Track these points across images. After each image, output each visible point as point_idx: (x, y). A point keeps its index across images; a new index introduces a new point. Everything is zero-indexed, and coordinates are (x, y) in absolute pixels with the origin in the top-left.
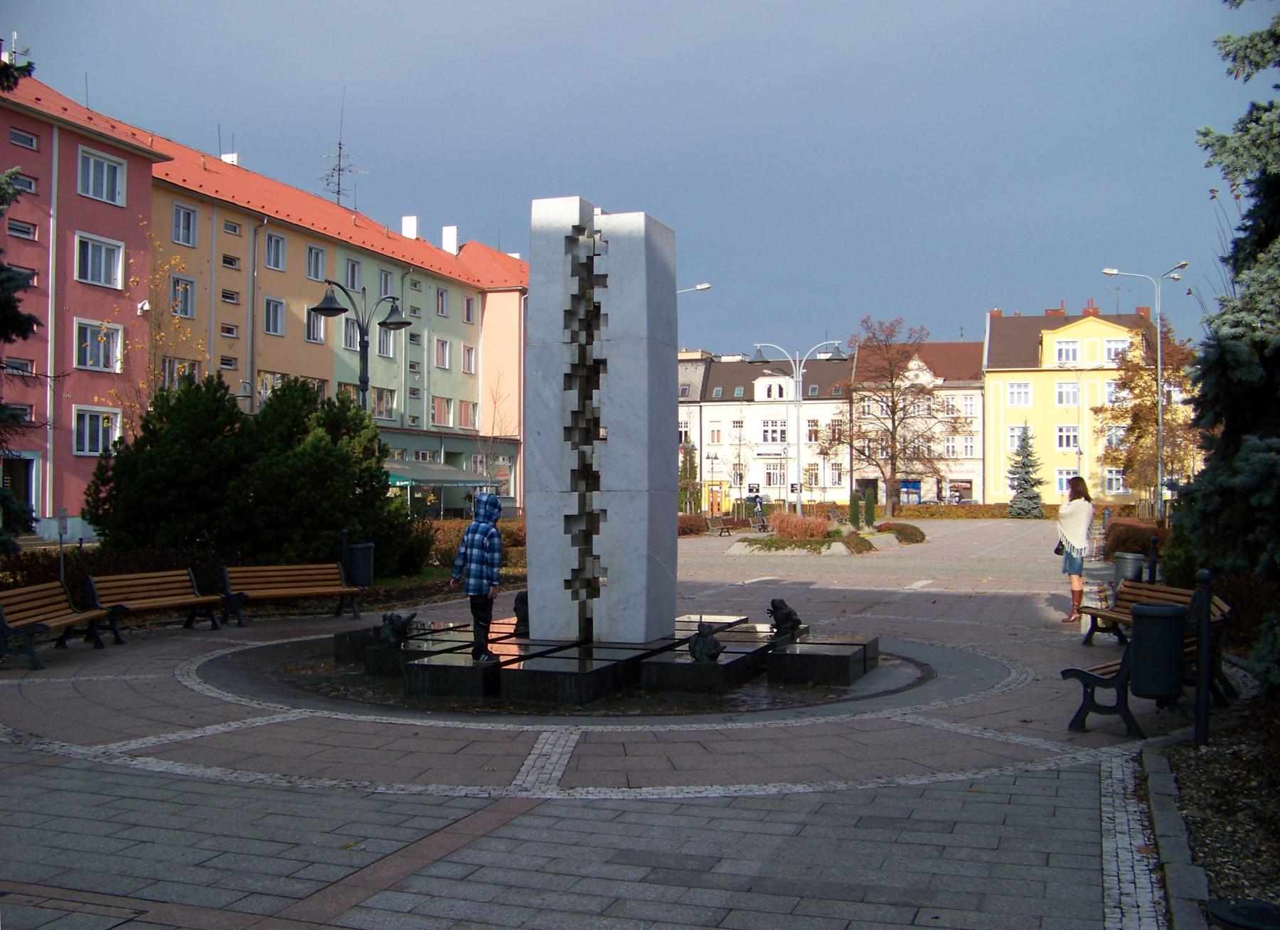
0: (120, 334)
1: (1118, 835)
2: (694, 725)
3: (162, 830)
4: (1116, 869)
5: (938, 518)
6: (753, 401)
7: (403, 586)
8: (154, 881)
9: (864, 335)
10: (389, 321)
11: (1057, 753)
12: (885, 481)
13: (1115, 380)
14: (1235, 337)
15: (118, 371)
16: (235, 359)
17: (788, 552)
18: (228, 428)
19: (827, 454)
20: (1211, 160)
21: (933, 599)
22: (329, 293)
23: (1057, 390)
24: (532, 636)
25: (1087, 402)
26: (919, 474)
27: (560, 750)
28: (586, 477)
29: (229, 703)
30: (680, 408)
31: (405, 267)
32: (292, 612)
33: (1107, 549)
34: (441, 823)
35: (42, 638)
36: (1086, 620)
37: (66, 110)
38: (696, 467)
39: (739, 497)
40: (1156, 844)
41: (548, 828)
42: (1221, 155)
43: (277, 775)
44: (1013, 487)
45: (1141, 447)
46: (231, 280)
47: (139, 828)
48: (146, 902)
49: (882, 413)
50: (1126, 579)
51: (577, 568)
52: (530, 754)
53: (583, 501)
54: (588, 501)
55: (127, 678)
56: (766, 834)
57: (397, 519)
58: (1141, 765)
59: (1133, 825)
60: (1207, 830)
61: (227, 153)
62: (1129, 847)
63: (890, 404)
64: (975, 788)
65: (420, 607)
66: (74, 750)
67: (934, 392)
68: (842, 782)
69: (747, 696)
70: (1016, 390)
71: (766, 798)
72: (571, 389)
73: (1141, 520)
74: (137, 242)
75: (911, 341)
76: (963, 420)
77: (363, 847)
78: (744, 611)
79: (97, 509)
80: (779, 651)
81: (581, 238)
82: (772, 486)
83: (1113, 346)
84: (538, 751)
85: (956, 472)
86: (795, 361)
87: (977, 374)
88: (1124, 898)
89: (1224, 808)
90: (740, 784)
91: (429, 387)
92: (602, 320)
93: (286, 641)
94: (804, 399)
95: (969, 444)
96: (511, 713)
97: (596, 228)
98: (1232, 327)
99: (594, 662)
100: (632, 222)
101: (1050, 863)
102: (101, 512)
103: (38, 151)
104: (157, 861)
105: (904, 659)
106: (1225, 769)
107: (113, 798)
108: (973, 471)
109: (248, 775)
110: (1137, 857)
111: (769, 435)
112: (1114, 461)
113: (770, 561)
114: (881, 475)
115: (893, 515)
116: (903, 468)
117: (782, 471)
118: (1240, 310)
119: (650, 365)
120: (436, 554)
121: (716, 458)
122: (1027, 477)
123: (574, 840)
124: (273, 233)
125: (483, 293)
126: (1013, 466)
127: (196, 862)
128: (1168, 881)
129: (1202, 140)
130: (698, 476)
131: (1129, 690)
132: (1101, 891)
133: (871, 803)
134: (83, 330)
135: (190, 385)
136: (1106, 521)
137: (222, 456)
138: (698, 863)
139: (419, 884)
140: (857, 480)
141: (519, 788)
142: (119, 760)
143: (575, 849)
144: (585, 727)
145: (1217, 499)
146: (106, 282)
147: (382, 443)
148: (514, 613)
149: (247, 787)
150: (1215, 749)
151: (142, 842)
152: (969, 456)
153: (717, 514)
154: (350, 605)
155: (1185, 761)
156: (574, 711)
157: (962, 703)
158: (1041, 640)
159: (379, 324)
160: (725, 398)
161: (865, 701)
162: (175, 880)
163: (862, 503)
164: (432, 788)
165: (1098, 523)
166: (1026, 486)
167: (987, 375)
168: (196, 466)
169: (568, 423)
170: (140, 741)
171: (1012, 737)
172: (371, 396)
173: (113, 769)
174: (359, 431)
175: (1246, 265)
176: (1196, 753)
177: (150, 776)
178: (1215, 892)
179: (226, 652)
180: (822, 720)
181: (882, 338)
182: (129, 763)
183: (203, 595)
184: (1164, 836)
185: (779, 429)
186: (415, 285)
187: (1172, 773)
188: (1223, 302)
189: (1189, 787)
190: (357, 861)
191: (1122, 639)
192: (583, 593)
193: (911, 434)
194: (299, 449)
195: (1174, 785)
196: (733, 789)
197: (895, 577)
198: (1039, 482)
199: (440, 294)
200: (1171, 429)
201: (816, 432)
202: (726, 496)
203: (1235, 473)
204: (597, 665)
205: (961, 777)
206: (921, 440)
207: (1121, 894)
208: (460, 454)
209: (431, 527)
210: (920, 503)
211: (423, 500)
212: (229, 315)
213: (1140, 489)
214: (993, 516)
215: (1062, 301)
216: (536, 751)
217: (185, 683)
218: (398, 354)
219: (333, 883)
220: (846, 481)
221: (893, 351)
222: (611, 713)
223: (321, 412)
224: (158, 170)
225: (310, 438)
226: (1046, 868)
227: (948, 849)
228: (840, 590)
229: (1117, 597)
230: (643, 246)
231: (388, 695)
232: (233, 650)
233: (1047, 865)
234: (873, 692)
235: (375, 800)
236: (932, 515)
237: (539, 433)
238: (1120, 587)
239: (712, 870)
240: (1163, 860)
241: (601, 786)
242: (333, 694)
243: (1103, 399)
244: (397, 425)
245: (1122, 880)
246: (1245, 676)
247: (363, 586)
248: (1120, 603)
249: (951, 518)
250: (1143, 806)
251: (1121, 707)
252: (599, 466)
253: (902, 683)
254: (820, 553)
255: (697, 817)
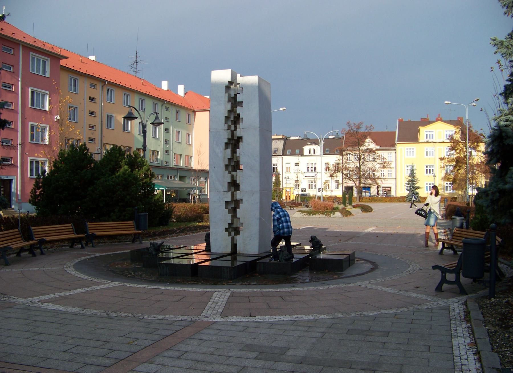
0: (48, 128)
1: (459, 338)
2: (278, 289)
3: (52, 336)
4: (459, 353)
5: (378, 202)
6: (303, 155)
7: (161, 230)
8: (46, 359)
9: (347, 129)
10: (154, 122)
11: (431, 301)
12: (356, 187)
13: (449, 147)
14: (506, 126)
15: (47, 143)
16: (94, 138)
17: (317, 216)
18: (88, 166)
19: (333, 176)
20: (497, 51)
21: (377, 236)
22: (130, 111)
23: (425, 151)
24: (212, 251)
25: (438, 155)
26: (370, 184)
27: (222, 300)
28: (234, 185)
29: (85, 279)
30: (273, 158)
31: (163, 101)
32: (114, 241)
33: (447, 215)
34: (170, 332)
35: (11, 252)
36: (441, 244)
37: (25, 38)
38: (280, 182)
39: (297, 194)
40: (476, 342)
41: (216, 335)
42: (501, 49)
43: (102, 311)
44: (407, 190)
45: (460, 173)
46: (93, 107)
47: (42, 335)
48: (41, 368)
49: (355, 160)
50: (457, 227)
51: (230, 223)
52: (209, 302)
53: (233, 195)
54: (235, 195)
55: (44, 269)
56: (308, 337)
57: (158, 203)
58: (466, 306)
59: (465, 333)
60: (497, 336)
61: (91, 55)
62: (464, 343)
63: (358, 156)
64: (397, 316)
65: (167, 239)
66: (19, 300)
67: (376, 152)
68: (341, 314)
69: (301, 276)
70: (409, 151)
71: (308, 321)
72: (228, 149)
73: (460, 203)
74: (54, 92)
75: (367, 131)
76: (388, 163)
77: (136, 343)
78: (299, 240)
79: (35, 199)
80: (314, 257)
81: (232, 86)
82: (311, 189)
83: (448, 133)
84: (213, 300)
85: (385, 183)
86: (320, 139)
87: (393, 144)
88: (463, 367)
89: (503, 326)
90: (298, 315)
91: (173, 150)
92: (240, 120)
93: (111, 253)
94: (324, 155)
95: (390, 173)
96: (202, 284)
97: (238, 82)
98: (505, 122)
99: (237, 262)
100: (253, 79)
101: (430, 350)
102: (37, 200)
103: (14, 55)
104: (48, 350)
105: (366, 260)
106: (503, 309)
107: (32, 321)
108: (392, 183)
109: (90, 311)
110: (468, 348)
111: (310, 169)
112: (449, 179)
113: (310, 219)
114: (355, 185)
115: (359, 201)
116: (363, 182)
117: (315, 183)
118: (508, 115)
119: (260, 139)
120: (174, 217)
121: (288, 178)
122: (413, 185)
123: (226, 340)
124: (109, 88)
125: (195, 112)
126: (408, 181)
127: (64, 350)
128: (482, 359)
129: (493, 42)
130: (281, 185)
131: (461, 273)
132: (453, 364)
133: (353, 323)
134: (32, 127)
135: (73, 149)
136: (446, 203)
137: (86, 177)
138: (279, 350)
139: (159, 360)
140: (345, 187)
141: (204, 317)
142: (38, 304)
143: (227, 344)
144: (233, 290)
145: (498, 194)
146: (42, 108)
147: (152, 172)
148: (205, 242)
149: (90, 316)
150: (498, 300)
151: (43, 341)
152: (390, 177)
153: (289, 201)
154: (138, 238)
155: (485, 305)
156: (229, 283)
157: (390, 279)
158: (421, 252)
159: (123, 118)
160: (292, 154)
161: (349, 278)
162: (55, 358)
163: (347, 196)
164: (167, 317)
165: (442, 204)
166: (413, 189)
167: (397, 145)
168: (75, 181)
169: (227, 163)
170: (47, 296)
171: (412, 294)
172: (148, 154)
173: (34, 309)
174: (142, 167)
175: (510, 96)
176: (490, 301)
177: (49, 312)
178: (503, 364)
179: (86, 258)
180: (332, 287)
181: (355, 130)
182: (41, 306)
183: (78, 234)
184: (479, 338)
185: (313, 166)
186: (167, 109)
187: (480, 310)
188: (501, 111)
189: (488, 316)
190: (133, 350)
191: (455, 252)
192: (233, 233)
193: (367, 168)
194: (117, 174)
195: (481, 316)
196: (294, 317)
197: (361, 226)
198: (418, 188)
199: (177, 112)
200: (472, 167)
201: (329, 168)
202: (292, 193)
203: (506, 183)
204: (238, 263)
205: (391, 312)
206: (371, 171)
207: (462, 365)
208: (185, 177)
209: (172, 206)
210: (370, 196)
211: (171, 195)
212: (91, 121)
213: (459, 190)
214: (400, 201)
215: (428, 115)
216: (212, 300)
217: (68, 271)
218: (160, 136)
219: (122, 360)
220: (340, 187)
221: (359, 135)
222: (243, 284)
223: (127, 159)
224: (63, 62)
225: (122, 170)
226: (429, 353)
227: (386, 344)
228: (339, 231)
229: (453, 235)
230: (257, 90)
231: (152, 276)
232: (89, 257)
233: (429, 351)
234: (353, 275)
235: (142, 322)
236: (375, 201)
237: (214, 167)
238: (454, 230)
239: (286, 354)
240: (479, 349)
241: (239, 316)
242: (129, 275)
243: (444, 154)
244: (160, 165)
245: (462, 358)
246: (507, 268)
247: (143, 230)
248: (454, 237)
249: (383, 202)
250: (469, 325)
251: (457, 281)
252: (239, 181)
253: (365, 270)
254: (330, 216)
255: (279, 329)
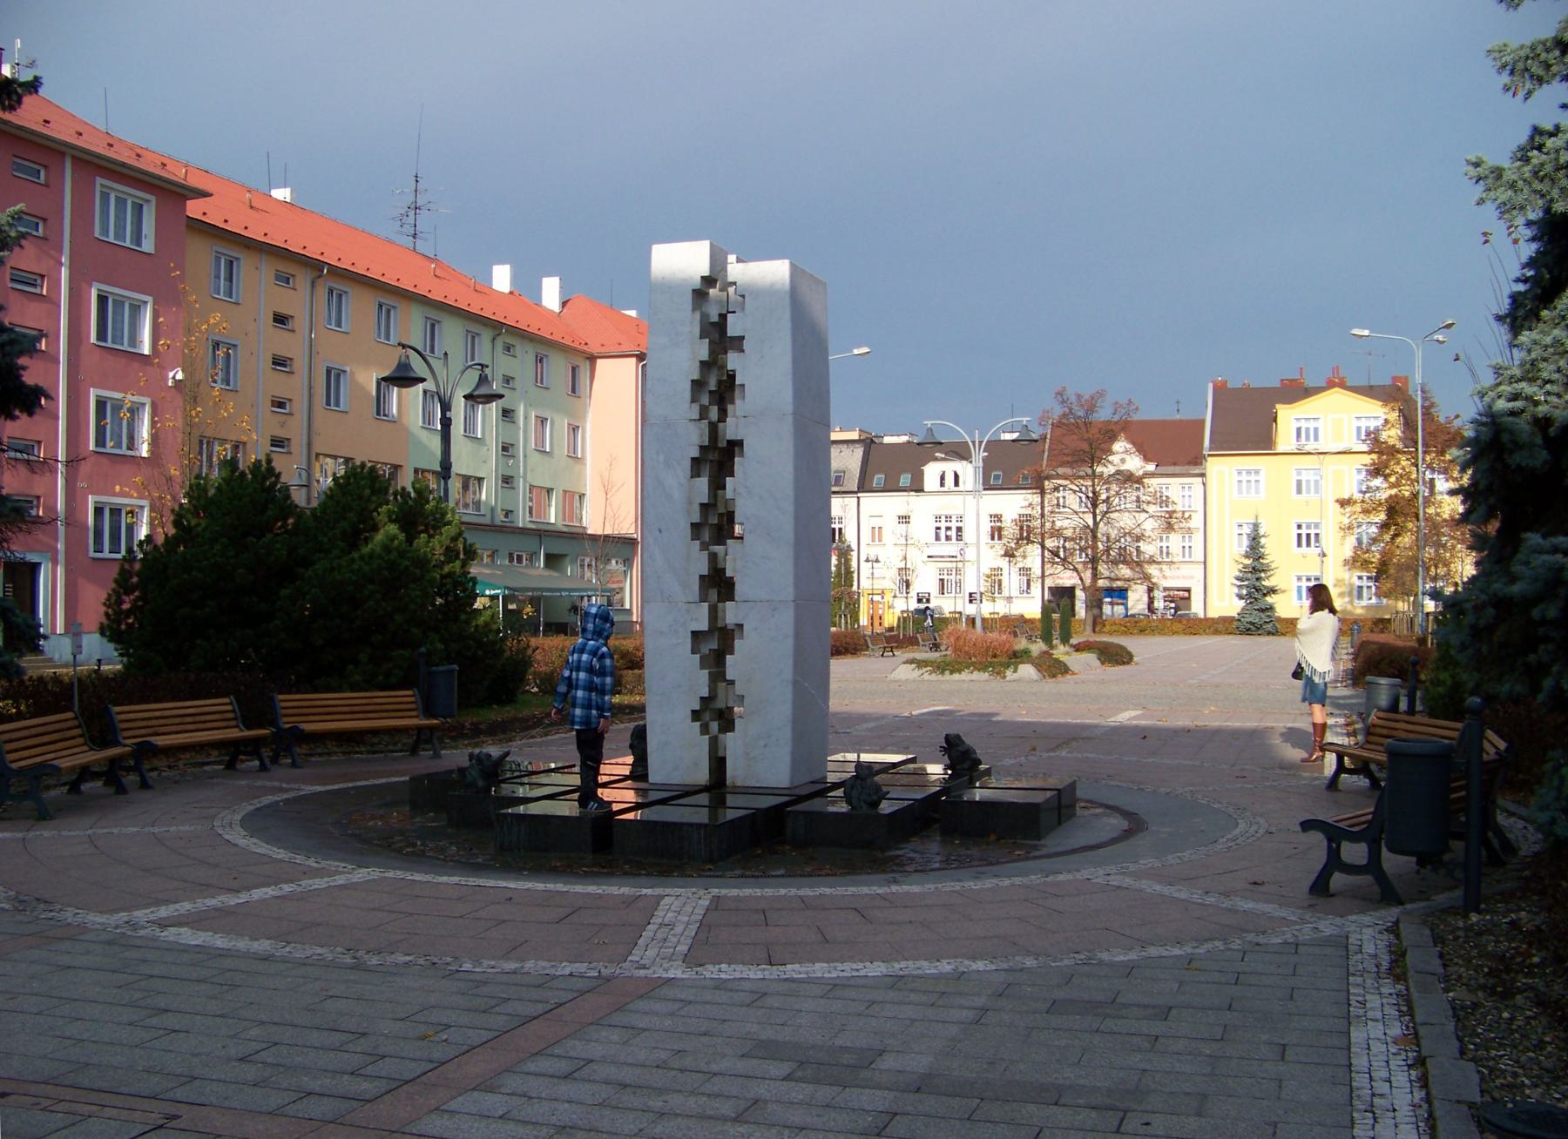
0: (148, 409)
1: (1369, 1022)
2: (850, 889)
3: (199, 1017)
4: (1367, 1064)
5: (1149, 634)
6: (922, 491)
7: (494, 718)
8: (189, 1079)
9: (1058, 411)
10: (476, 393)
11: (1295, 923)
12: (1084, 589)
13: (1366, 465)
14: (1512, 413)
15: (145, 454)
16: (288, 439)
17: (965, 675)
18: (279, 524)
19: (1013, 556)
20: (1484, 196)
21: (1142, 734)
22: (403, 358)
23: (1295, 477)
24: (652, 779)
25: (1332, 492)
26: (1125, 580)
27: (686, 919)
28: (718, 584)
29: (281, 861)
30: (833, 500)
31: (496, 327)
32: (358, 749)
33: (1356, 672)
34: (540, 1008)
35: (52, 782)
36: (1331, 760)
37: (80, 134)
38: (853, 572)
39: (905, 609)
40: (1416, 1034)
41: (672, 1014)
42: (1495, 189)
43: (339, 949)
44: (1240, 597)
45: (1398, 547)
46: (283, 343)
47: (170, 1014)
48: (179, 1105)
49: (1080, 506)
50: (1380, 710)
51: (707, 695)
52: (649, 923)
53: (714, 614)
54: (720, 614)
55: (156, 830)
56: (938, 1021)
57: (487, 636)
58: (1398, 936)
59: (1387, 1010)
60: (1478, 1016)
61: (278, 187)
62: (1383, 1037)
63: (1091, 495)
64: (1194, 965)
65: (514, 743)
66: (91, 918)
67: (1145, 480)
68: (1032, 958)
69: (916, 852)
70: (1244, 477)
71: (938, 978)
72: (699, 476)
73: (1397, 637)
74: (168, 297)
75: (1116, 418)
76: (1179, 515)
77: (445, 1037)
78: (911, 749)
79: (119, 624)
80: (954, 797)
81: (712, 291)
82: (946, 595)
83: (1364, 424)
84: (660, 920)
85: (1171, 578)
86: (974, 442)
87: (1196, 458)
88: (1376, 1100)
89: (1499, 989)
90: (907, 960)
91: (525, 474)
92: (737, 392)
93: (350, 785)
94: (985, 489)
95: (1187, 544)
96: (626, 874)
97: (730, 279)
98: (1510, 400)
99: (728, 810)
100: (774, 271)
101: (1287, 1057)
102: (123, 627)
103: (47, 185)
104: (193, 1055)
105: (1107, 807)
106: (1501, 942)
107: (139, 977)
108: (1192, 577)
109: (304, 950)
110: (1393, 1049)
111: (942, 533)
112: (1365, 564)
113: (943, 686)
114: (1080, 582)
115: (1094, 631)
116: (1106, 573)
117: (958, 577)
118: (1520, 380)
119: (796, 447)
120: (534, 678)
121: (877, 561)
122: (1257, 584)
123: (703, 1029)
124: (334, 285)
125: (592, 359)
126: (1241, 571)
127: (240, 1056)
128: (1430, 1079)
129: (1472, 171)
130: (855, 583)
131: (1383, 845)
132: (1349, 1091)
133: (1067, 983)
134: (101, 404)
135: (233, 471)
136: (1355, 638)
137: (272, 558)
138: (855, 1057)
139: (513, 1082)
140: (1050, 588)
141: (636, 965)
142: (146, 931)
143: (704, 1039)
144: (717, 890)
145: (1490, 611)
146: (130, 346)
147: (468, 543)
148: (630, 751)
149: (303, 963)
150: (1488, 917)
151: (174, 1031)
152: (1187, 559)
153: (878, 630)
154: (429, 741)
155: (1452, 932)
156: (703, 871)
157: (1179, 861)
158: (1275, 783)
159: (464, 397)
160: (888, 488)
161: (1060, 858)
162: (214, 1077)
163: (1055, 616)
164: (529, 965)
165: (1345, 641)
166: (1257, 595)
167: (1209, 459)
168: (240, 571)
169: (696, 518)
170: (172, 907)
171: (1240, 903)
172: (455, 485)
173: (138, 942)
174: (440, 528)
175: (1527, 324)
176: (1465, 923)
177: (184, 951)
178: (1488, 1092)
179: (277, 798)
180: (1007, 882)
181: (1081, 413)
182: (158, 934)
183: (249, 728)
184: (1425, 1024)
185: (954, 525)
186: (508, 349)
187: (1436, 946)
188: (1498, 370)
189: (1456, 964)
190: (437, 1055)
191: (1375, 783)
192: (714, 726)
193: (1116, 532)
194: (366, 550)
195: (1438, 962)
196: (898, 967)
197: (1097, 707)
198: (1273, 591)
199: (540, 360)
200: (1435, 526)
201: (1000, 529)
202: (889, 607)
203: (1513, 579)
204: (731, 815)
205: (1177, 952)
206: (1129, 539)
207: (1373, 1095)
208: (563, 556)
209: (528, 646)
210: (1127, 616)
211: (518, 612)
212: (280, 385)
213: (1397, 599)
214: (1217, 632)
215: (1301, 369)
216: (656, 920)
217: (226, 837)
218: (487, 433)
219: (407, 1082)
220: (1036, 589)
221: (1094, 430)
222: (748, 873)
223: (393, 505)
224: (194, 208)
225: (380, 537)
226: (1281, 1063)
227: (1161, 1040)
228: (1029, 723)
229: (1368, 731)
230: (787, 301)
231: (475, 851)
232: (285, 796)
233: (1283, 1059)
234: (1069, 848)
235: (459, 980)
236: (1142, 631)
237: (660, 531)
238: (1372, 719)
239: (873, 1066)
240: (1424, 1053)
241: (736, 962)
242: (408, 850)
243: (1351, 489)
244: (487, 521)
245: (1375, 1078)
246: (1525, 827)
247: (445, 718)
248: (1372, 738)
249: (1165, 634)
250: (1400, 987)
251: (1373, 866)
252: (734, 571)
253: (1105, 836)
254: (1004, 677)
255: (854, 1000)
